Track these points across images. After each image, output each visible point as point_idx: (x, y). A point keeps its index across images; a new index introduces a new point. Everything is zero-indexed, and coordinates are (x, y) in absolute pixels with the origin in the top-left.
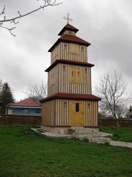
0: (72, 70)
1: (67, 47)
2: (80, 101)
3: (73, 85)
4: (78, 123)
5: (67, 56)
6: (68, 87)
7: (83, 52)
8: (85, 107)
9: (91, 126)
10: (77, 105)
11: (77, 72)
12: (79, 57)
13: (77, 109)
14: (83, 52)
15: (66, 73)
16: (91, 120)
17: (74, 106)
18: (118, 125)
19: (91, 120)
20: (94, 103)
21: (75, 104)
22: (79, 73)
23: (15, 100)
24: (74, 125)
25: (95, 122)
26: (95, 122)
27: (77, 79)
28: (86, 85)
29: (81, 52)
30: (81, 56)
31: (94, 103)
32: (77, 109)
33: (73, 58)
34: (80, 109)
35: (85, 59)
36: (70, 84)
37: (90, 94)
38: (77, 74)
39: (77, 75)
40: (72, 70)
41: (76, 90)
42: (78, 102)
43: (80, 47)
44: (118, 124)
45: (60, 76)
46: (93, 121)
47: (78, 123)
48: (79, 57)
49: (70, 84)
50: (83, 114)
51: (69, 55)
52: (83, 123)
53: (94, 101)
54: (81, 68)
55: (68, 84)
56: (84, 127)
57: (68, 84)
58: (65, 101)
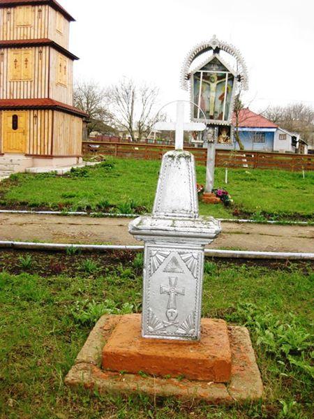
0: (14, 57)
1: (12, 15)
2: (20, 111)
3: (15, 83)
4: (15, 149)
5: (12, 32)
6: (8, 88)
7: (40, 20)
8: (28, 121)
9: (39, 153)
10: (15, 118)
11: (23, 59)
12: (32, 31)
13: (15, 126)
14: (40, 20)
15: (5, 64)
16: (39, 144)
17: (11, 119)
18: (245, 163)
19: (39, 144)
20: (46, 113)
21: (11, 118)
22: (26, 61)
23: (251, 141)
24: (9, 151)
25: (46, 147)
26: (46, 147)
27: (22, 71)
28: (40, 82)
29: (36, 19)
30: (36, 28)
31: (46, 113)
32: (15, 126)
33: (22, 35)
34: (20, 125)
35: (43, 33)
36: (12, 83)
37: (46, 97)
38: (23, 62)
39: (23, 65)
40: (14, 57)
41: (22, 92)
42: (17, 113)
43: (34, 11)
44: (246, 160)
45: (36, 72)
46: (42, 145)
47: (15, 149)
48: (32, 31)
49: (12, 83)
50: (24, 133)
51: (15, 29)
52: (23, 149)
53: (47, 111)
54: (30, 52)
55: (8, 83)
56: (26, 155)
57: (8, 83)
58: (36, 112)
